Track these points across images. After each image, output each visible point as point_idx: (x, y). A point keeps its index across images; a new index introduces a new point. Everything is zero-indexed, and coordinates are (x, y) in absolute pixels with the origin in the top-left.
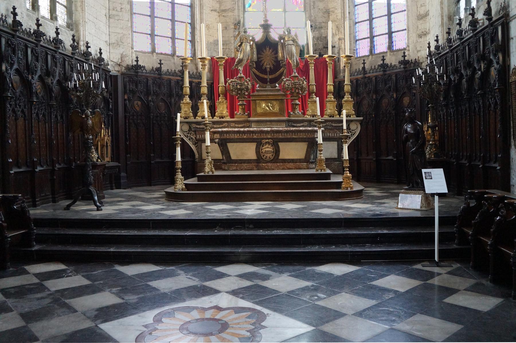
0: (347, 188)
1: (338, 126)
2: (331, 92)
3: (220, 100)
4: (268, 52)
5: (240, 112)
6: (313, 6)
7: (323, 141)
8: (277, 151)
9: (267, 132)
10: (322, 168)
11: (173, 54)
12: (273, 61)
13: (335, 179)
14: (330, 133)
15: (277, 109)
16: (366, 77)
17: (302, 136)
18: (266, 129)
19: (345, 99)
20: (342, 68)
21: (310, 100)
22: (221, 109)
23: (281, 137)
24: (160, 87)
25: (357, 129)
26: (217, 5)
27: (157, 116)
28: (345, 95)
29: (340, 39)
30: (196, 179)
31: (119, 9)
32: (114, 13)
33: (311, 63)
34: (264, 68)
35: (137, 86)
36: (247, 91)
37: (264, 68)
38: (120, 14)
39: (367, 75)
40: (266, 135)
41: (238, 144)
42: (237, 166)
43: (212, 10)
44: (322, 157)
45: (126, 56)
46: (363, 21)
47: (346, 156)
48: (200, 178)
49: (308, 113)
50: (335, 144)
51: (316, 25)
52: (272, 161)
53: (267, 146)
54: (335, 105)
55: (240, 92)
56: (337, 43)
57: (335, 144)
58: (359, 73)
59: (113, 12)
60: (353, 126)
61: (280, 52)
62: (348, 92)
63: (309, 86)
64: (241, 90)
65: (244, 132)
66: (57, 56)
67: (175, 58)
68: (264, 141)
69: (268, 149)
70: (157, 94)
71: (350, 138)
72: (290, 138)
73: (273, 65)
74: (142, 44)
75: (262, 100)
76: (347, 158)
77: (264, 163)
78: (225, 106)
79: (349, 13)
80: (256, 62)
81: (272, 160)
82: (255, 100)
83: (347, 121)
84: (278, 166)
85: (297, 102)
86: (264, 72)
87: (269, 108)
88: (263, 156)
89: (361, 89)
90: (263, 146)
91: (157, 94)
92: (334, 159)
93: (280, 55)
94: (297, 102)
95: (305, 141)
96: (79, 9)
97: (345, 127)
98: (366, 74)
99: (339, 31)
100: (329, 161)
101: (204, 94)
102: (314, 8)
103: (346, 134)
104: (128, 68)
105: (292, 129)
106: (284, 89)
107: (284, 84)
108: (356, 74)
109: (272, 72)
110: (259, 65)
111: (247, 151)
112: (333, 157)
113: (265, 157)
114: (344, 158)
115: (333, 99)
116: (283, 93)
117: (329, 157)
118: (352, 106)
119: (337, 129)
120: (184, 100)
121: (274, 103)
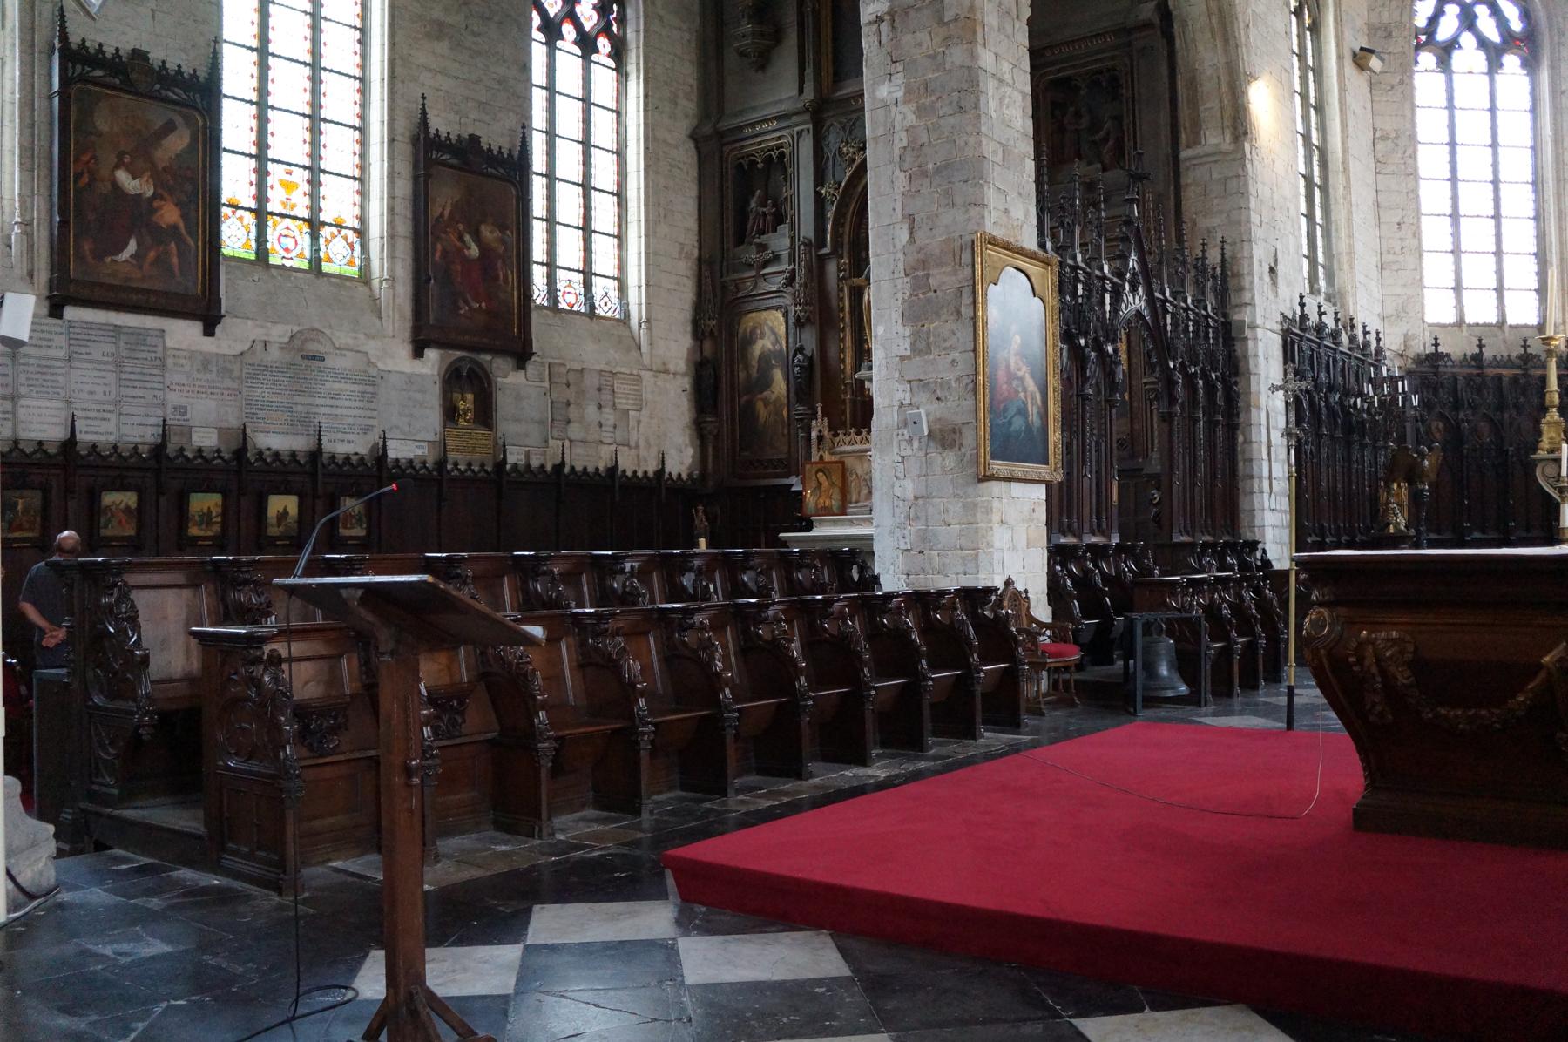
11: (1460, 323)
24: (1479, 391)
27: (1475, 450)
31: (1398, 250)
32: (1391, 258)
35: (1435, 394)
38: (1401, 258)
45: (1414, 337)
59: (1388, 258)
66: (1338, 357)
67: (1464, 328)
70: (1473, 407)
74: (1439, 310)
91: (1473, 407)
96: (1346, 267)
104: (1419, 360)
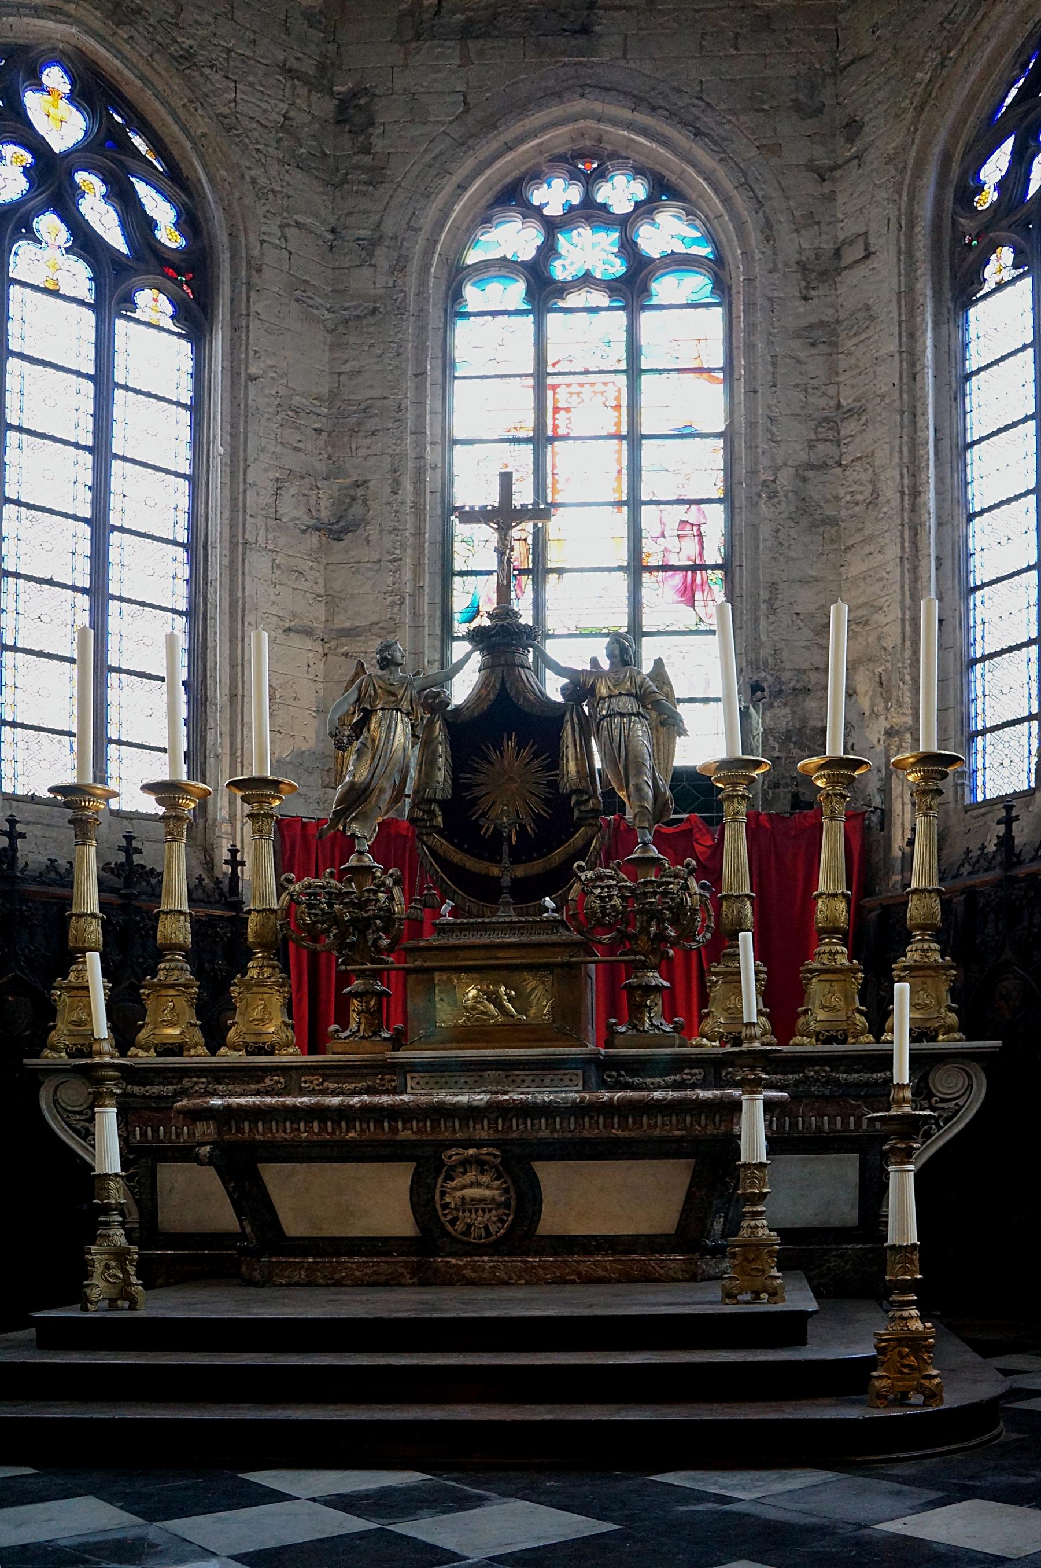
0: (905, 1395)
1: (867, 1084)
2: (832, 931)
3: (253, 973)
4: (512, 757)
5: (353, 1026)
6: (769, 601)
7: (769, 1152)
8: (527, 1200)
9: (470, 1112)
10: (758, 1283)
12: (533, 802)
13: (826, 1347)
15: (541, 1004)
16: (1014, 879)
17: (660, 1128)
19: (912, 956)
20: (897, 853)
21: (721, 968)
22: (256, 1013)
23: (544, 1134)
25: (967, 1096)
26: (320, 612)
28: (908, 939)
29: (889, 733)
30: (30, 1333)
33: (730, 798)
34: (487, 829)
36: (386, 930)
37: (487, 829)
39: (1021, 872)
42: (311, 1269)
43: (289, 629)
44: (763, 1233)
46: (1010, 650)
47: (903, 1224)
48: (54, 1336)
50: (846, 1168)
51: (778, 679)
52: (495, 1247)
53: (471, 1176)
54: (856, 987)
55: (352, 938)
56: (880, 748)
57: (846, 1168)
58: (982, 861)
60: (946, 1083)
61: (570, 753)
62: (923, 928)
64: (362, 925)
65: (344, 1113)
68: (453, 1155)
71: (928, 1135)
72: (600, 1139)
73: (538, 819)
75: (467, 969)
76: (913, 1238)
77: (453, 1255)
78: (277, 1000)
79: (940, 621)
80: (443, 804)
82: (430, 970)
84: (530, 1269)
85: (654, 978)
86: (489, 847)
87: (500, 1006)
88: (453, 1222)
89: (990, 930)
90: (450, 1178)
92: (841, 1234)
93: (572, 767)
94: (654, 978)
98: (1020, 863)
99: (887, 700)
100: (803, 1249)
101: (174, 948)
102: (773, 611)
103: (907, 1110)
105: (606, 1096)
107: (584, 893)
108: (966, 870)
110: (458, 814)
111: (379, 1202)
112: (835, 1222)
113: (460, 1226)
116: (577, 937)
117: (815, 1223)
118: (944, 988)
119: (865, 1098)
120: (72, 977)
121: (530, 982)
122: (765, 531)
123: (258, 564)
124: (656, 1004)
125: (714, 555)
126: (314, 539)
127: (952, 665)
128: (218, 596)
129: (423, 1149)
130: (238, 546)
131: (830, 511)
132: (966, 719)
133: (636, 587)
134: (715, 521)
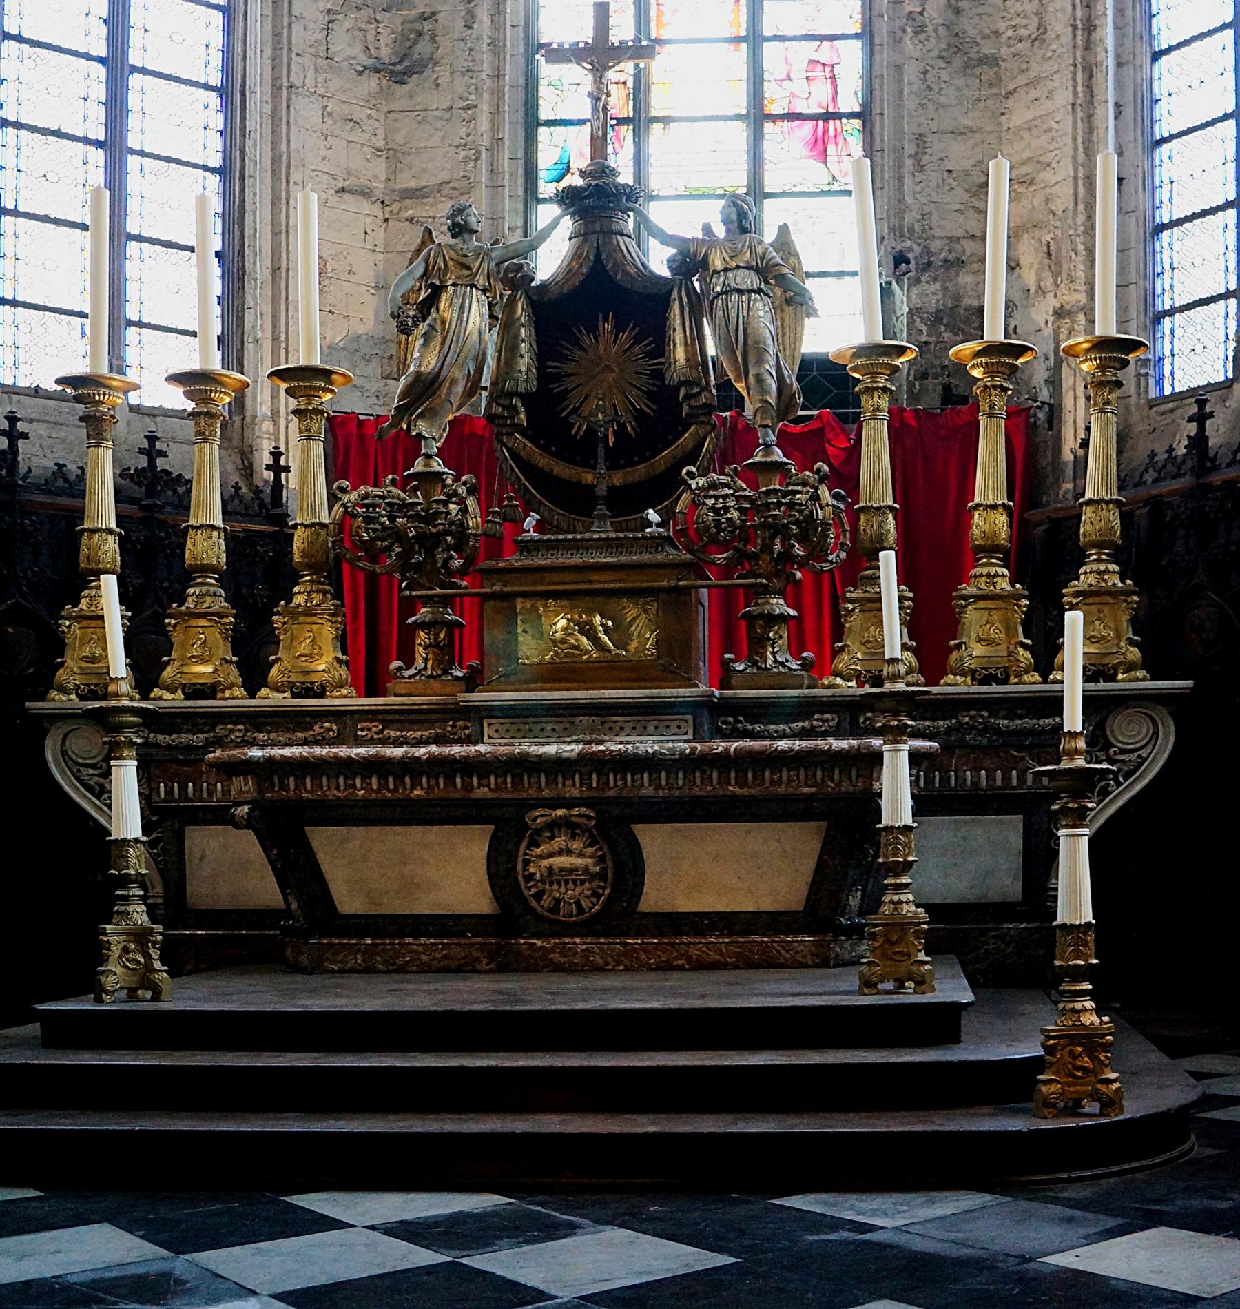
1: (1032, 732)
3: (300, 600)
4: (608, 341)
5: (420, 663)
8: (627, 870)
9: (559, 765)
10: (902, 970)
14: (976, 769)
15: (644, 637)
16: (1209, 488)
17: (786, 784)
18: (551, 749)
19: (1086, 579)
20: (1067, 456)
21: (858, 594)
22: (304, 648)
23: (648, 791)
25: (1152, 748)
26: (380, 168)
28: (1081, 559)
29: (1059, 313)
33: (869, 391)
34: (579, 428)
36: (458, 547)
37: (579, 428)
39: (1216, 479)
40: (552, 782)
41: (374, 830)
42: (369, 952)
46: (1203, 214)
47: (1075, 900)
48: (63, 1032)
49: (842, 662)
50: (1008, 832)
51: (927, 250)
52: (589, 927)
53: (560, 842)
54: (1019, 617)
56: (1048, 331)
57: (1008, 832)
60: (1126, 731)
61: (678, 337)
62: (1099, 545)
63: (854, 517)
64: (429, 543)
65: (408, 767)
68: (539, 816)
69: (564, 858)
71: (1105, 793)
73: (639, 415)
75: (546, 595)
76: (1087, 915)
78: (328, 632)
79: (1120, 180)
80: (526, 398)
81: (596, 918)
83: (1090, 702)
84: (630, 952)
86: (582, 450)
87: (593, 638)
88: (538, 896)
93: (680, 354)
94: (778, 605)
95: (806, 816)
97: (1073, 718)
98: (1215, 468)
99: (1056, 274)
100: (957, 929)
101: (205, 569)
102: (921, 168)
103: (1080, 762)
106: (700, 539)
107: (695, 505)
108: (1150, 477)
109: (622, 455)
110: (547, 409)
111: (450, 873)
112: (994, 896)
113: (546, 901)
114: (1062, 917)
115: (1004, 585)
116: (686, 556)
118: (1125, 618)
119: (1029, 748)
120: (84, 604)
121: (631, 611)
122: (911, 71)
123: (306, 111)
124: (780, 637)
125: (850, 101)
126: (372, 82)
127: (1134, 233)
128: (258, 150)
129: (502, 809)
130: (281, 89)
131: (988, 49)
132: (1150, 297)
133: (757, 137)
134: (850, 61)
